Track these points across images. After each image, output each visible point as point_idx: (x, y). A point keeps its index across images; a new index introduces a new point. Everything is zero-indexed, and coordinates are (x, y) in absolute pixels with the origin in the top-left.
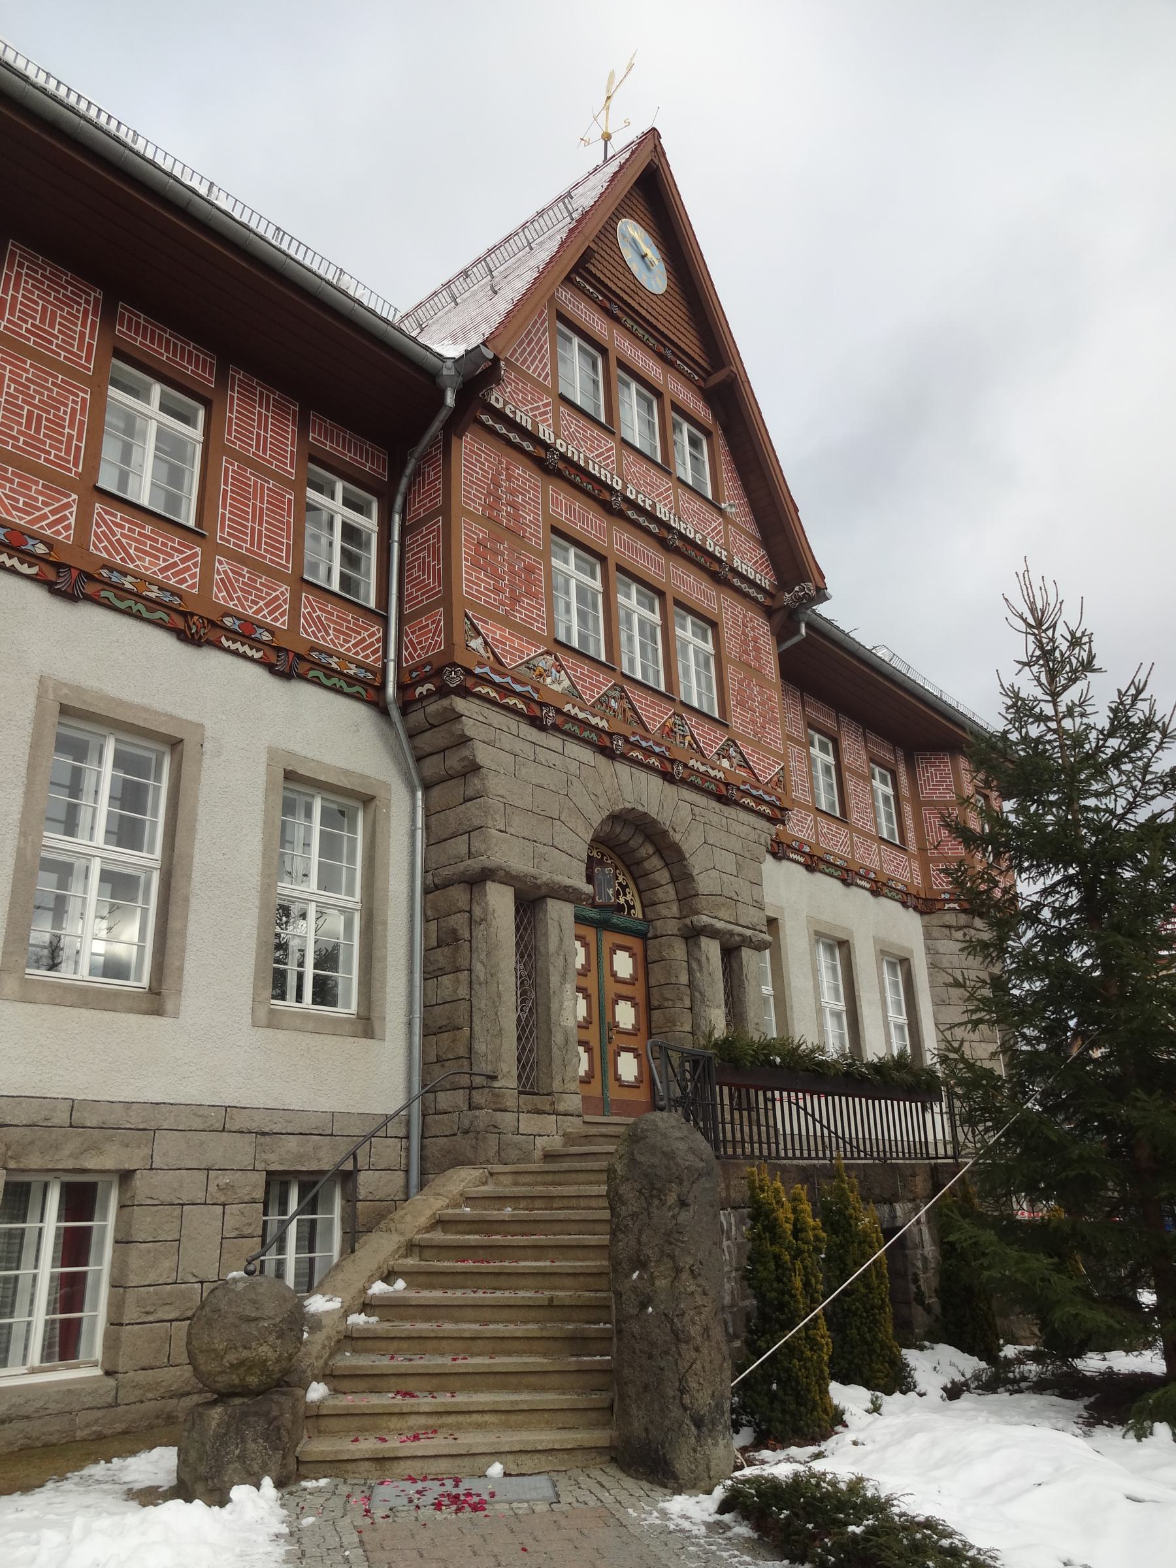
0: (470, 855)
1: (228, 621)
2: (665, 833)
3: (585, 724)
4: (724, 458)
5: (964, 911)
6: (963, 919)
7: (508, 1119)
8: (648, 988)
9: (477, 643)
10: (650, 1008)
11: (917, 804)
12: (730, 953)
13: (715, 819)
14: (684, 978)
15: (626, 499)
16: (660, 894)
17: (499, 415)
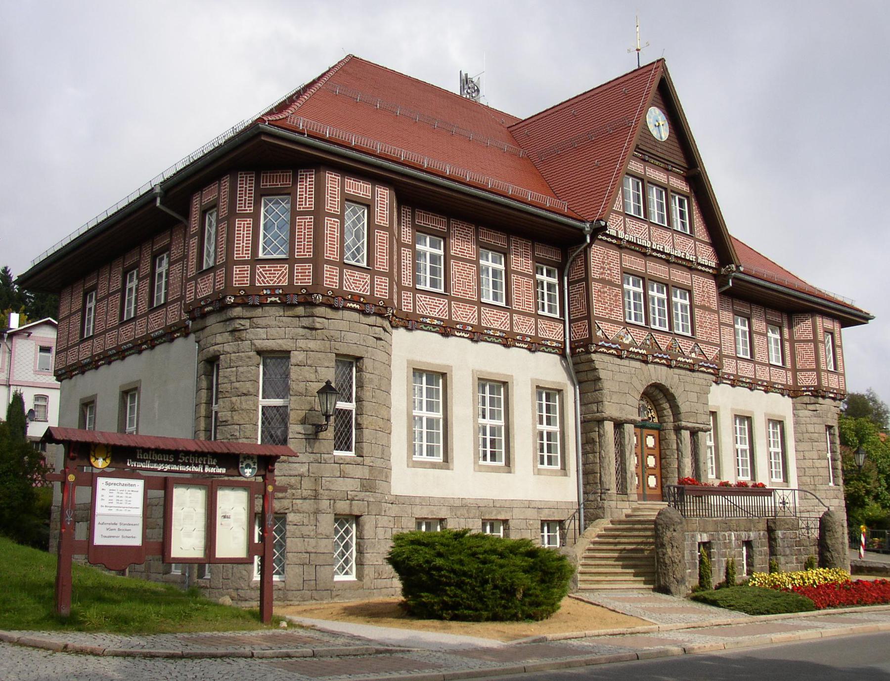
0: (598, 412)
1: (458, 326)
2: (668, 390)
4: (695, 207)
5: (813, 395)
6: (813, 399)
7: (613, 504)
8: (660, 450)
9: (599, 333)
10: (661, 459)
11: (792, 341)
12: (694, 433)
13: (688, 379)
14: (675, 446)
15: (652, 249)
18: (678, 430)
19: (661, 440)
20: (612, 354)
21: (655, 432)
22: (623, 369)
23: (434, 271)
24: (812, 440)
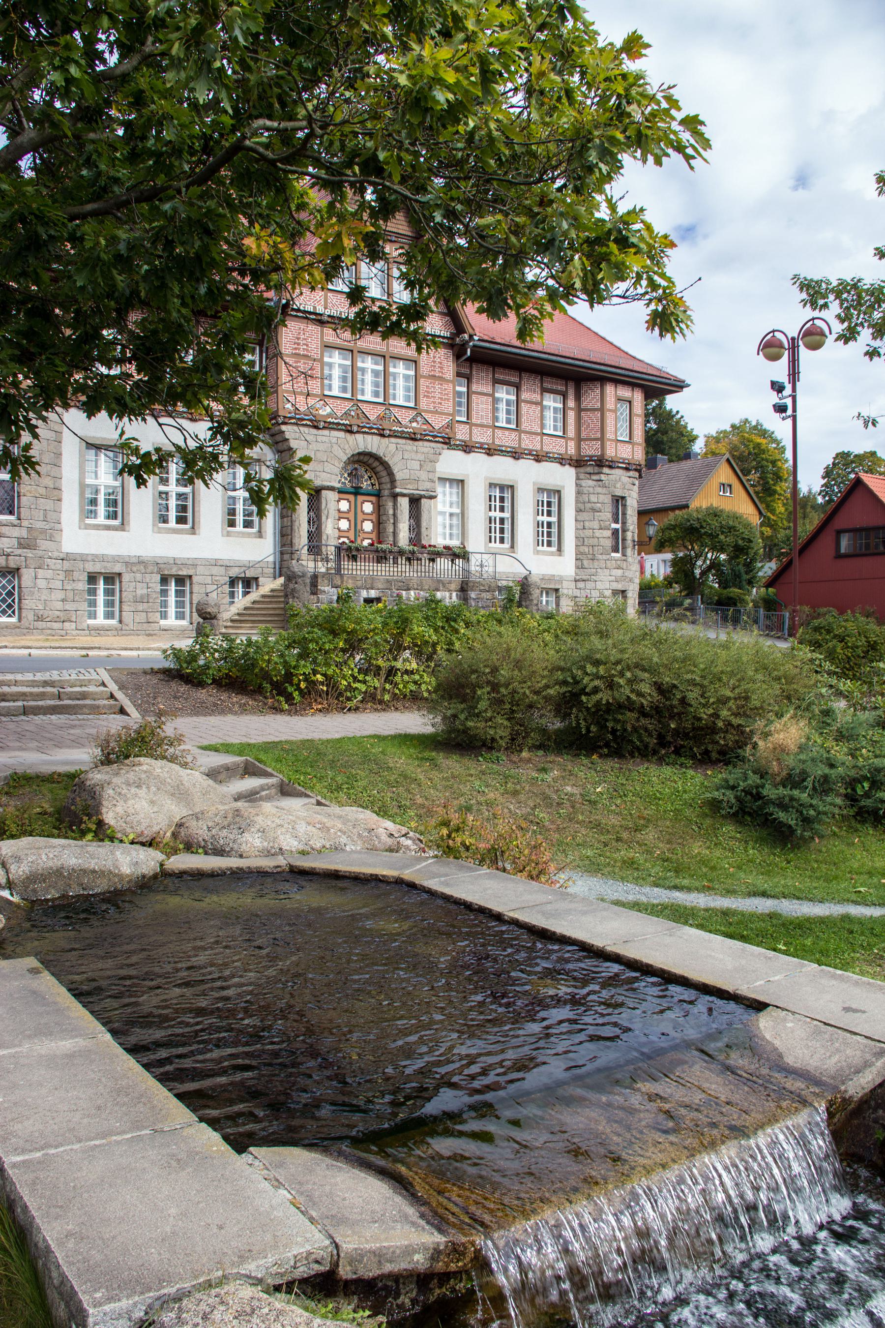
3: (338, 424)
6: (596, 469)
11: (579, 410)
13: (409, 448)
14: (391, 512)
16: (383, 480)
17: (298, 310)
18: (395, 496)
19: (379, 509)
20: (306, 425)
21: (373, 499)
22: (319, 439)
23: (508, 412)
24: (594, 510)
